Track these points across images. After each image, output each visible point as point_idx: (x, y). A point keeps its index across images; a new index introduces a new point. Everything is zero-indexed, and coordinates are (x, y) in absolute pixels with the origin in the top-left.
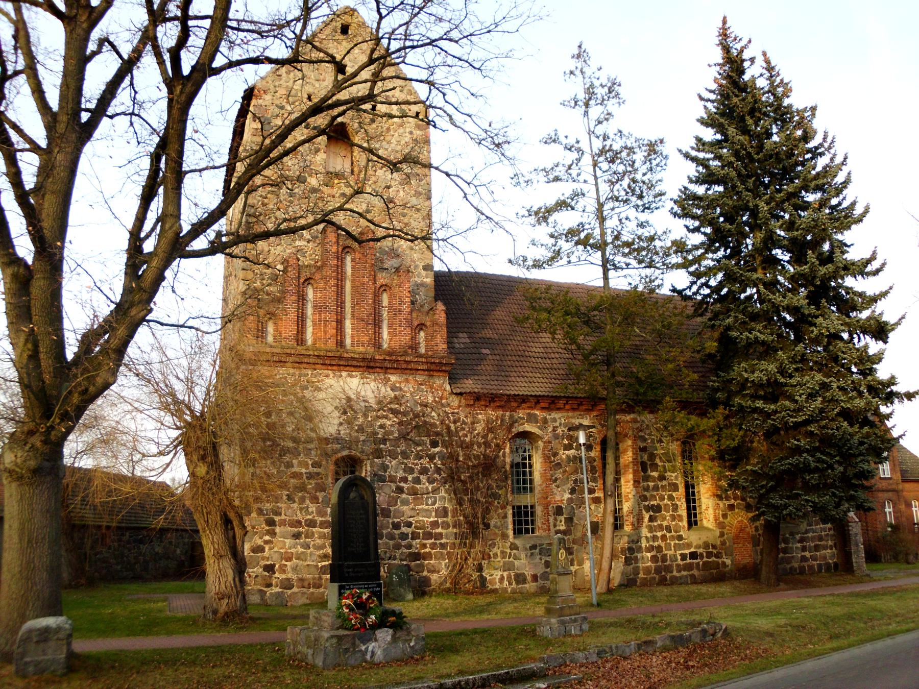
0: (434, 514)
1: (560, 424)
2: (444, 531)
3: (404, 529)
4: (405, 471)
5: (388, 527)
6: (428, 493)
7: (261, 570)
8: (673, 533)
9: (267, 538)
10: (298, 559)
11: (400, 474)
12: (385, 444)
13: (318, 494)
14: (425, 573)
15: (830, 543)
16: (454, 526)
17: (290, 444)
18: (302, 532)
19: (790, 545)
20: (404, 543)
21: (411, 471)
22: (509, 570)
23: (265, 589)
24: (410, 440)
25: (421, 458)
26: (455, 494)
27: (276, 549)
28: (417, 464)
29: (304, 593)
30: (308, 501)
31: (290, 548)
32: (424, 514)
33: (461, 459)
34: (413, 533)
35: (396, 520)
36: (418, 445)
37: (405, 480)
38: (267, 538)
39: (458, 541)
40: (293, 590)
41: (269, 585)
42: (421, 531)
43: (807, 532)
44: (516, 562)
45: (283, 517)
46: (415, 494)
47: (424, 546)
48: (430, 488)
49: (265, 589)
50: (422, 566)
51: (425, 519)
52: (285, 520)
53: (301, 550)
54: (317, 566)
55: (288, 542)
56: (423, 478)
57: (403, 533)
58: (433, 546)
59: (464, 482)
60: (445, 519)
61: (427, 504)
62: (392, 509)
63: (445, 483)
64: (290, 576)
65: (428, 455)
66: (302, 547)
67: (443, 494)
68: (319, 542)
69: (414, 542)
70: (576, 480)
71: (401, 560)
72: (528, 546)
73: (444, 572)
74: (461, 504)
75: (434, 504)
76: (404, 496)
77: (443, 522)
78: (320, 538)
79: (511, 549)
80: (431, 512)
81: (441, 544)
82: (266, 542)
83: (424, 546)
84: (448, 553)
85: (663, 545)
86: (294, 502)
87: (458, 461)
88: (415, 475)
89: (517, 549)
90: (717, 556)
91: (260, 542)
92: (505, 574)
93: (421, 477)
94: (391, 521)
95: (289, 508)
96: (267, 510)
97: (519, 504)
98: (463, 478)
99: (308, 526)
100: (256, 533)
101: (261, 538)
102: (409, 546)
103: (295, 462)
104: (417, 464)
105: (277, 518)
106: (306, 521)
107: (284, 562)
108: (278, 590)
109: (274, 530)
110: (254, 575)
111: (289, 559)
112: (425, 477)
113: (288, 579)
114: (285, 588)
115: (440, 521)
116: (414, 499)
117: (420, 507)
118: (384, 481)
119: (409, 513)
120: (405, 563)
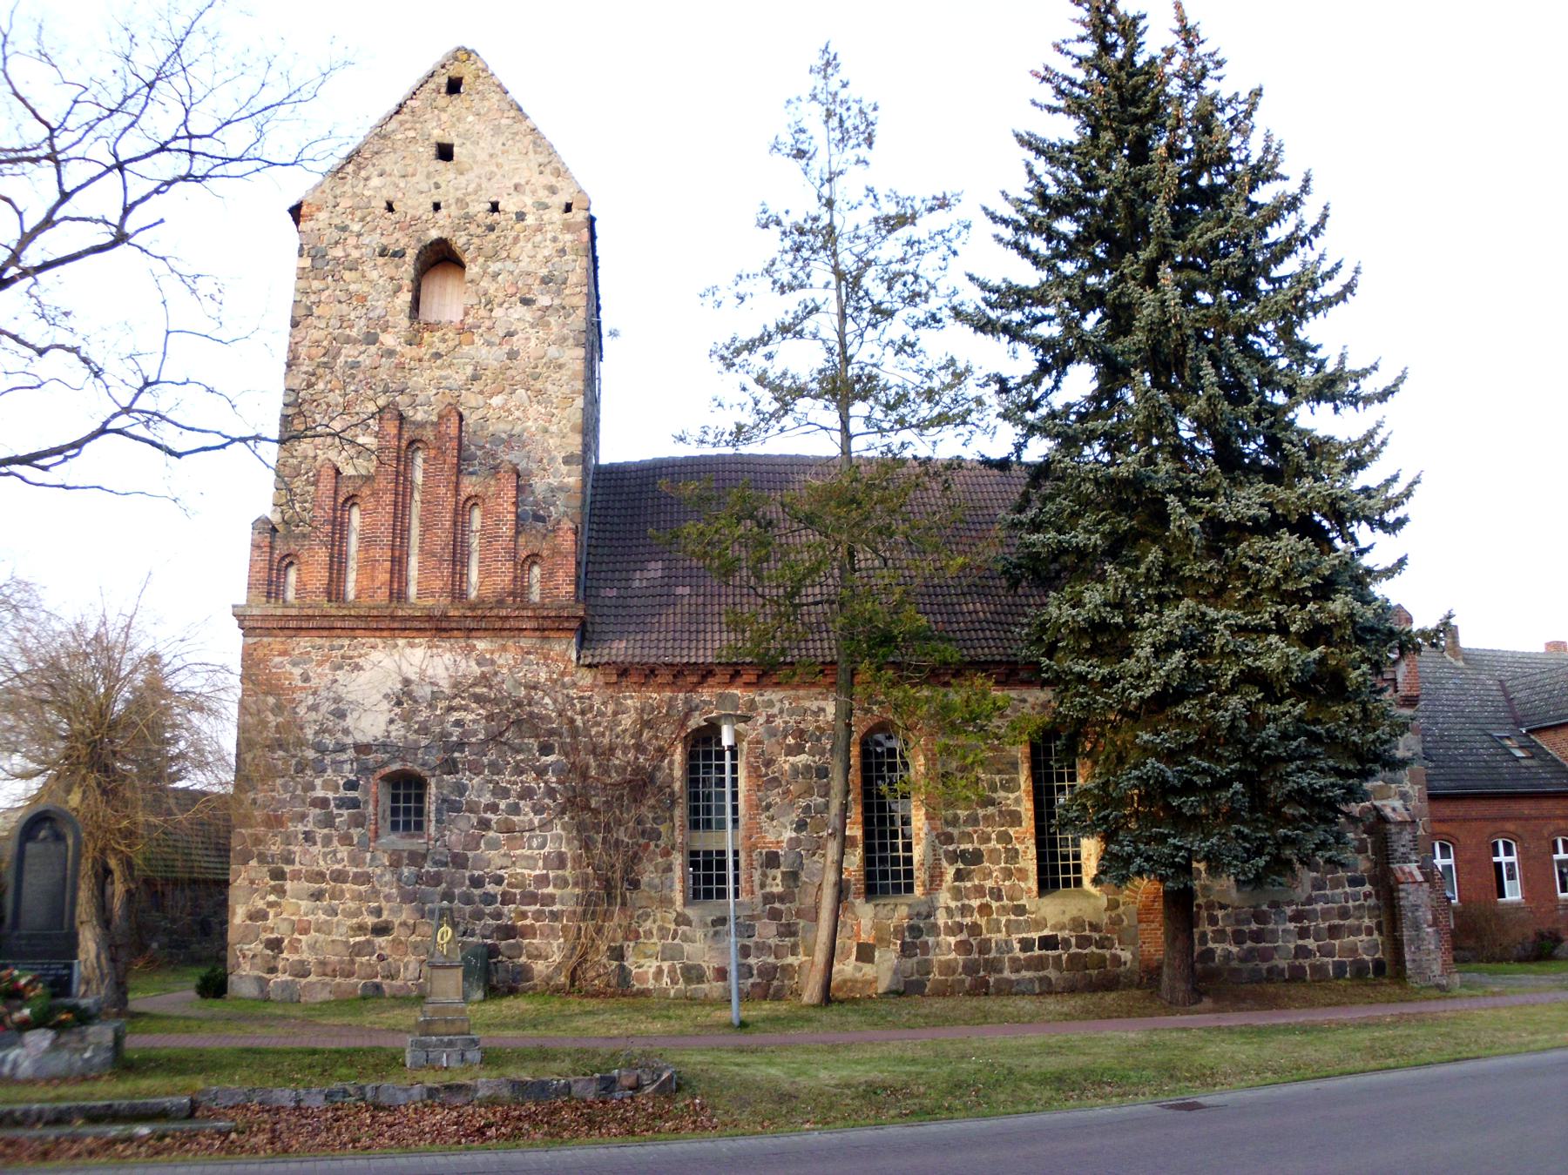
0: (541, 863)
1: (781, 711)
3: (490, 888)
4: (494, 793)
5: (462, 884)
7: (261, 946)
8: (1005, 902)
9: (272, 898)
10: (318, 930)
11: (486, 799)
12: (462, 751)
14: (523, 959)
15: (1367, 922)
16: (576, 884)
17: (311, 754)
18: (326, 890)
19: (1271, 926)
20: (488, 910)
21: (505, 793)
22: (672, 959)
23: (267, 976)
24: (505, 744)
25: (522, 773)
26: (578, 831)
28: (515, 783)
29: (325, 984)
30: (335, 842)
31: (306, 914)
32: (524, 863)
34: (504, 894)
35: (476, 873)
36: (518, 752)
37: (493, 808)
38: (272, 898)
39: (579, 909)
40: (309, 979)
41: (273, 970)
42: (518, 891)
43: (1310, 900)
44: (686, 946)
45: (297, 866)
47: (524, 915)
49: (267, 976)
50: (519, 947)
51: (526, 872)
52: (300, 871)
53: (323, 917)
54: (347, 942)
55: (305, 904)
56: (525, 805)
58: (538, 916)
59: (596, 812)
61: (530, 848)
62: (470, 854)
63: (563, 812)
64: (305, 956)
65: (534, 768)
67: (558, 830)
68: (352, 905)
69: (506, 909)
70: (808, 806)
71: (484, 937)
72: (709, 919)
73: (557, 958)
75: (542, 846)
76: (491, 834)
77: (556, 878)
78: (353, 899)
79: (678, 924)
80: (536, 860)
82: (271, 905)
83: (524, 915)
85: (983, 922)
86: (315, 843)
87: (584, 776)
88: (511, 800)
89: (688, 923)
90: (1101, 944)
91: (261, 904)
92: (666, 966)
93: (522, 803)
94: (467, 874)
95: (305, 852)
96: (273, 856)
97: (709, 848)
100: (257, 890)
101: (263, 898)
103: (318, 782)
104: (515, 783)
105: (287, 868)
106: (332, 872)
107: (296, 936)
108: (286, 977)
109: (282, 886)
110: (250, 954)
111: (305, 931)
112: (529, 803)
113: (302, 962)
114: (296, 976)
115: (551, 874)
117: (518, 852)
118: (459, 810)
119: (499, 862)
120: (489, 941)
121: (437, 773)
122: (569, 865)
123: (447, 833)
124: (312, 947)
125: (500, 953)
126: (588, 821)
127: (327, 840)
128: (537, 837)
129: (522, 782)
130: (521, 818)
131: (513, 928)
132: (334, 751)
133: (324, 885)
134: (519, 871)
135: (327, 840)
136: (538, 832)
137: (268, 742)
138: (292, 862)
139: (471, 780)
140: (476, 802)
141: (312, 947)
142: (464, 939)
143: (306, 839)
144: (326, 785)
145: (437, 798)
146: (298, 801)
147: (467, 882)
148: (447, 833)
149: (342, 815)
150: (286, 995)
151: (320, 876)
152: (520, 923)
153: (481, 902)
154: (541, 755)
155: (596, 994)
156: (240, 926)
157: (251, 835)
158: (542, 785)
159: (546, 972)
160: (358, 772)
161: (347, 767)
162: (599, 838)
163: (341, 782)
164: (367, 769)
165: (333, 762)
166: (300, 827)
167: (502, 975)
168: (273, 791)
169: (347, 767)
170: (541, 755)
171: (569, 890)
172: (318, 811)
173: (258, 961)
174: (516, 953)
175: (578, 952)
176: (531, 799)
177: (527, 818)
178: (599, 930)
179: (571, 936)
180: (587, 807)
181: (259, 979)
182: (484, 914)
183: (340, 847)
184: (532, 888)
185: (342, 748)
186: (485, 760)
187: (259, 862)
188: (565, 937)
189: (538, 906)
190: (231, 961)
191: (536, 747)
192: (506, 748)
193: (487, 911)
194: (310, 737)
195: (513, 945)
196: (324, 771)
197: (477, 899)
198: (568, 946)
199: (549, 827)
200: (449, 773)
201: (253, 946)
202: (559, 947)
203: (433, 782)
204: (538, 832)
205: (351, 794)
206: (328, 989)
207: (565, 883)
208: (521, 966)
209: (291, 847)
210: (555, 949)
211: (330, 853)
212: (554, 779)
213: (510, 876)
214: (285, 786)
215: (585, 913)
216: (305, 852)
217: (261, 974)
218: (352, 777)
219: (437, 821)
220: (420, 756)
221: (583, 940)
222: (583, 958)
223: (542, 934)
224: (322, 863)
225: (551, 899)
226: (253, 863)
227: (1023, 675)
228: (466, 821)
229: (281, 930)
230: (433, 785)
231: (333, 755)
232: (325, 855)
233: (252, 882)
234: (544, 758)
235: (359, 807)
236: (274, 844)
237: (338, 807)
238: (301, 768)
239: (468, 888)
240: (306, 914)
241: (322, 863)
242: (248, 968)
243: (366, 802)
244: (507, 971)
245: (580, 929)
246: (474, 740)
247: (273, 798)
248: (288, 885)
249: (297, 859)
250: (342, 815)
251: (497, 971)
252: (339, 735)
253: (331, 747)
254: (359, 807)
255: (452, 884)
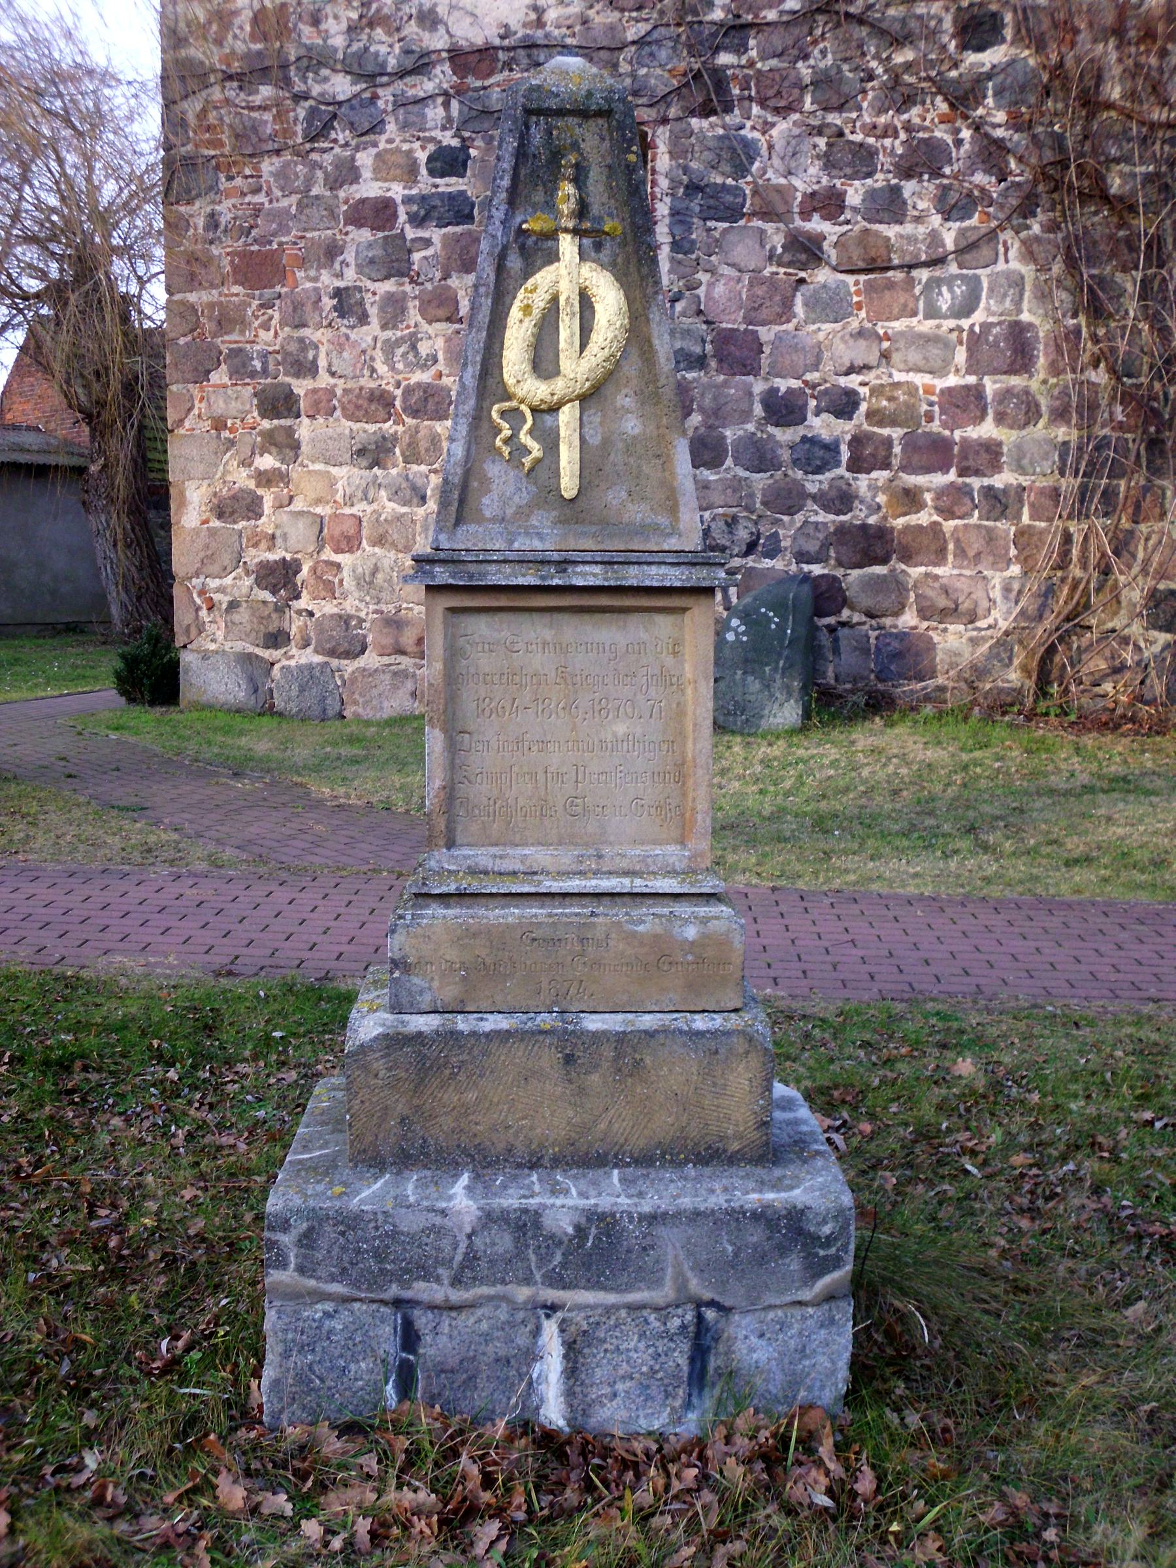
0: (961, 356)
2: (1007, 436)
3: (822, 425)
4: (829, 163)
5: (746, 415)
6: (937, 262)
7: (248, 581)
9: (267, 462)
10: (380, 541)
12: (741, 49)
13: (454, 282)
14: (909, 619)
16: (1060, 415)
17: (342, 86)
18: (395, 438)
20: (814, 484)
23: (266, 654)
24: (860, 20)
25: (908, 101)
26: (1071, 263)
27: (298, 505)
28: (889, 131)
29: (400, 675)
30: (414, 315)
31: (350, 501)
32: (914, 357)
33: (1114, 92)
34: (857, 441)
35: (784, 385)
36: (898, 41)
38: (267, 462)
39: (1069, 484)
40: (361, 662)
41: (277, 639)
42: (896, 433)
45: (324, 380)
46: (876, 266)
47: (911, 499)
48: (949, 240)
49: (266, 654)
50: (895, 585)
51: (920, 380)
52: (331, 392)
53: (392, 507)
55: (347, 476)
57: (810, 441)
59: (1124, 207)
60: (1016, 381)
62: (766, 333)
63: (1027, 209)
64: (350, 606)
65: (941, 87)
66: (395, 495)
67: (1014, 263)
69: (862, 483)
71: (802, 557)
73: (1001, 617)
74: (1097, 312)
75: (966, 308)
76: (823, 275)
77: (1005, 395)
80: (949, 348)
81: (988, 491)
82: (266, 479)
83: (911, 499)
84: (1023, 533)
86: (363, 319)
87: (1091, 103)
88: (879, 180)
91: (243, 479)
93: (909, 187)
94: (759, 387)
95: (340, 346)
96: (264, 356)
98: (1115, 185)
99: (415, 413)
100: (232, 443)
101: (246, 463)
102: (842, 500)
103: (365, 159)
104: (889, 131)
105: (301, 387)
106: (408, 391)
107: (328, 554)
108: (310, 657)
109: (290, 431)
110: (223, 599)
111: (349, 543)
112: (930, 187)
113: (345, 620)
114: (332, 653)
115: (991, 386)
116: (870, 287)
117: (898, 325)
118: (733, 214)
119: (847, 352)
120: (817, 570)
121: (673, 112)
122: (1042, 362)
123: (703, 277)
124: (367, 582)
125: (845, 602)
126: (1098, 233)
127: (394, 309)
128: (950, 281)
129: (908, 127)
130: (908, 228)
131: (881, 534)
132: (402, 74)
133: (389, 427)
134: (899, 377)
135: (394, 309)
136: (953, 268)
137: (236, 67)
138: (311, 370)
139: (766, 127)
140: (778, 189)
141: (367, 582)
142: (750, 562)
143: (342, 310)
144: (383, 167)
145: (675, 183)
146: (316, 213)
147: (758, 410)
148: (703, 277)
149: (427, 243)
150: (311, 699)
151: (381, 401)
152: (900, 522)
153: (795, 462)
154: (963, 47)
155: (1109, 723)
156: (196, 532)
157: (211, 305)
158: (966, 134)
159: (968, 656)
160: (465, 123)
161: (435, 113)
162: (1130, 283)
163: (422, 156)
164: (486, 113)
165: (401, 103)
166: (327, 280)
167: (849, 659)
168: (256, 191)
169: (435, 113)
170: (963, 47)
171: (1040, 430)
172: (365, 235)
173: (243, 616)
174: (887, 603)
175: (1062, 601)
176: (936, 173)
177: (922, 230)
178: (1122, 545)
179: (1044, 558)
180: (1099, 195)
181: (247, 659)
182: (804, 495)
183: (424, 326)
184: (935, 427)
185: (420, 64)
186: (804, 71)
187: (234, 373)
188: (1026, 560)
189: (952, 476)
190: (182, 616)
191: (948, 24)
192: (864, 31)
193: (812, 488)
194: (338, 41)
195: (880, 580)
196: (376, 128)
197: (785, 455)
198: (1034, 585)
199: (985, 252)
200: (706, 111)
201: (228, 580)
202: (1007, 589)
203: (662, 138)
204: (953, 268)
205: (451, 184)
206: (409, 685)
207: (1030, 412)
208: (902, 636)
209: (305, 332)
210: (997, 594)
211: (399, 342)
212: (1000, 117)
213: (876, 391)
214: (282, 175)
215: (1084, 494)
216: (340, 346)
217: (251, 649)
218: (449, 139)
219: (676, 246)
220: (624, 68)
221: (1076, 571)
222: (1074, 620)
223: (961, 552)
224: (382, 369)
225: (991, 453)
226: (220, 376)
227: (368, 212)
228: (751, 242)
229: (292, 542)
230: (662, 148)
231: (399, 85)
232: (389, 348)
233: (219, 424)
234: (972, 58)
235: (469, 218)
236: (266, 326)
237: (417, 221)
238: (319, 130)
239: (760, 426)
240: (350, 501)
241: (382, 369)
242: (220, 635)
243: (488, 203)
244: (866, 651)
245: (1067, 538)
246: (771, 15)
247: (257, 210)
248: (304, 429)
249: (322, 363)
250: (427, 243)
251: (836, 651)
252: (412, 29)
253: (392, 62)
254: (469, 218)
255: (717, 415)
